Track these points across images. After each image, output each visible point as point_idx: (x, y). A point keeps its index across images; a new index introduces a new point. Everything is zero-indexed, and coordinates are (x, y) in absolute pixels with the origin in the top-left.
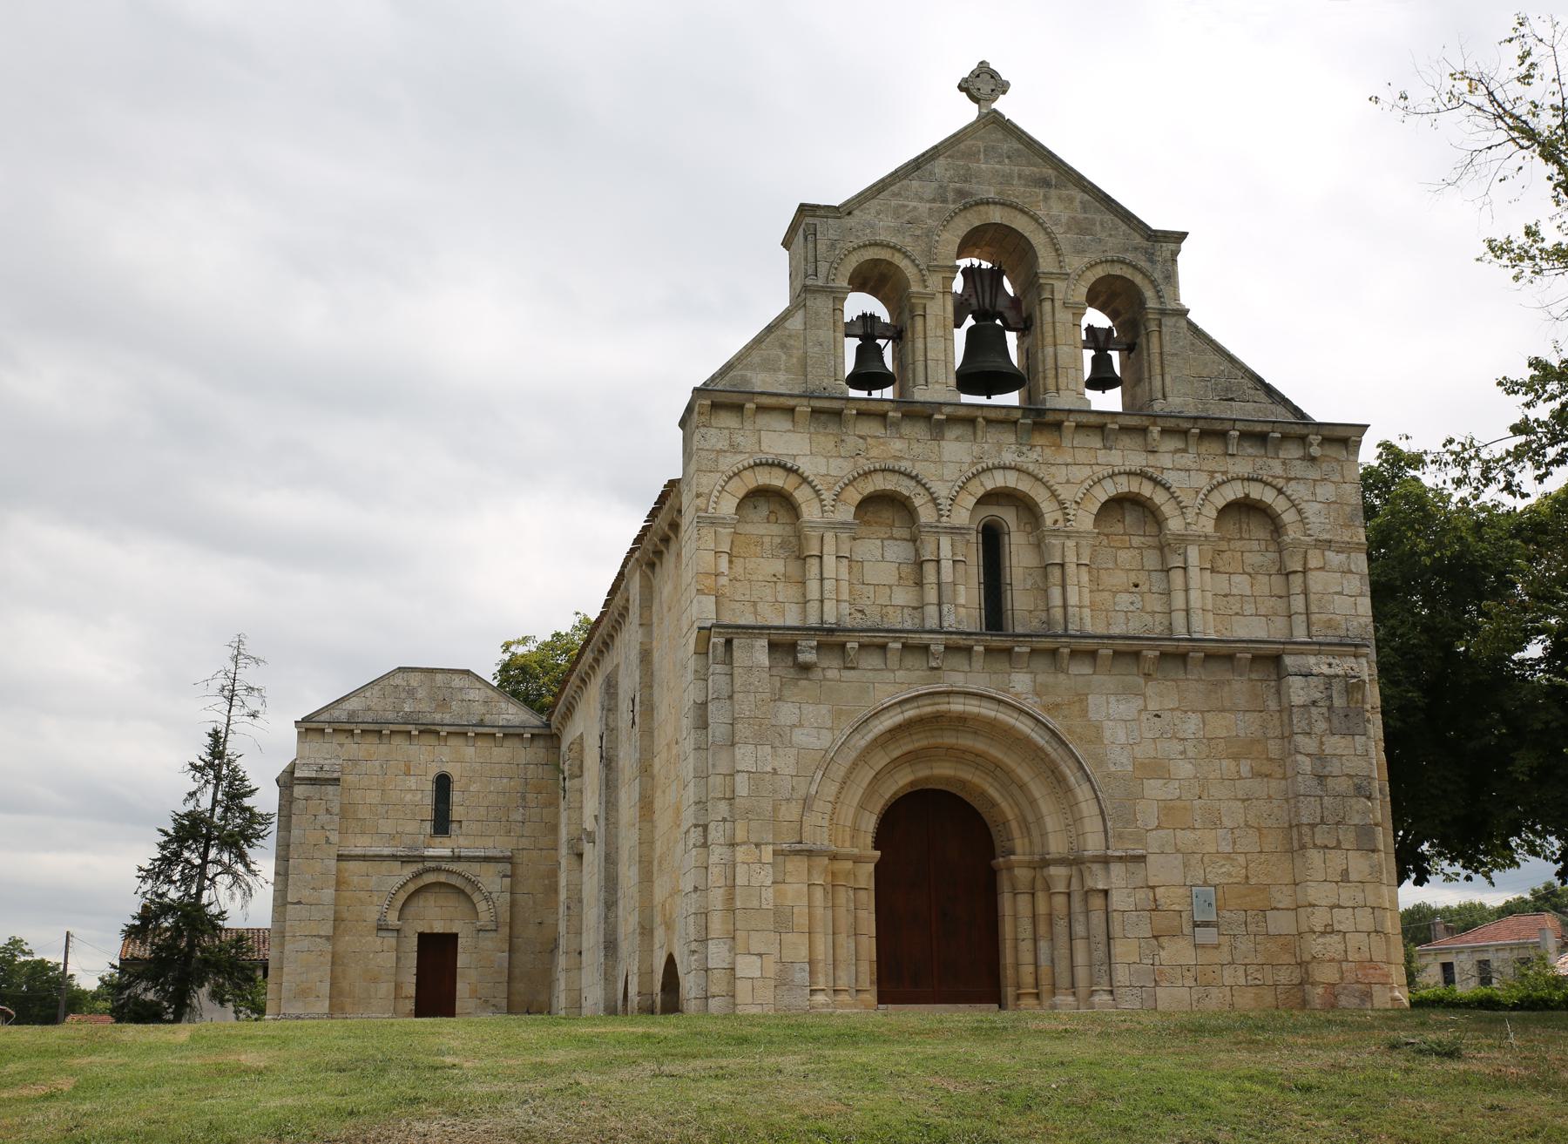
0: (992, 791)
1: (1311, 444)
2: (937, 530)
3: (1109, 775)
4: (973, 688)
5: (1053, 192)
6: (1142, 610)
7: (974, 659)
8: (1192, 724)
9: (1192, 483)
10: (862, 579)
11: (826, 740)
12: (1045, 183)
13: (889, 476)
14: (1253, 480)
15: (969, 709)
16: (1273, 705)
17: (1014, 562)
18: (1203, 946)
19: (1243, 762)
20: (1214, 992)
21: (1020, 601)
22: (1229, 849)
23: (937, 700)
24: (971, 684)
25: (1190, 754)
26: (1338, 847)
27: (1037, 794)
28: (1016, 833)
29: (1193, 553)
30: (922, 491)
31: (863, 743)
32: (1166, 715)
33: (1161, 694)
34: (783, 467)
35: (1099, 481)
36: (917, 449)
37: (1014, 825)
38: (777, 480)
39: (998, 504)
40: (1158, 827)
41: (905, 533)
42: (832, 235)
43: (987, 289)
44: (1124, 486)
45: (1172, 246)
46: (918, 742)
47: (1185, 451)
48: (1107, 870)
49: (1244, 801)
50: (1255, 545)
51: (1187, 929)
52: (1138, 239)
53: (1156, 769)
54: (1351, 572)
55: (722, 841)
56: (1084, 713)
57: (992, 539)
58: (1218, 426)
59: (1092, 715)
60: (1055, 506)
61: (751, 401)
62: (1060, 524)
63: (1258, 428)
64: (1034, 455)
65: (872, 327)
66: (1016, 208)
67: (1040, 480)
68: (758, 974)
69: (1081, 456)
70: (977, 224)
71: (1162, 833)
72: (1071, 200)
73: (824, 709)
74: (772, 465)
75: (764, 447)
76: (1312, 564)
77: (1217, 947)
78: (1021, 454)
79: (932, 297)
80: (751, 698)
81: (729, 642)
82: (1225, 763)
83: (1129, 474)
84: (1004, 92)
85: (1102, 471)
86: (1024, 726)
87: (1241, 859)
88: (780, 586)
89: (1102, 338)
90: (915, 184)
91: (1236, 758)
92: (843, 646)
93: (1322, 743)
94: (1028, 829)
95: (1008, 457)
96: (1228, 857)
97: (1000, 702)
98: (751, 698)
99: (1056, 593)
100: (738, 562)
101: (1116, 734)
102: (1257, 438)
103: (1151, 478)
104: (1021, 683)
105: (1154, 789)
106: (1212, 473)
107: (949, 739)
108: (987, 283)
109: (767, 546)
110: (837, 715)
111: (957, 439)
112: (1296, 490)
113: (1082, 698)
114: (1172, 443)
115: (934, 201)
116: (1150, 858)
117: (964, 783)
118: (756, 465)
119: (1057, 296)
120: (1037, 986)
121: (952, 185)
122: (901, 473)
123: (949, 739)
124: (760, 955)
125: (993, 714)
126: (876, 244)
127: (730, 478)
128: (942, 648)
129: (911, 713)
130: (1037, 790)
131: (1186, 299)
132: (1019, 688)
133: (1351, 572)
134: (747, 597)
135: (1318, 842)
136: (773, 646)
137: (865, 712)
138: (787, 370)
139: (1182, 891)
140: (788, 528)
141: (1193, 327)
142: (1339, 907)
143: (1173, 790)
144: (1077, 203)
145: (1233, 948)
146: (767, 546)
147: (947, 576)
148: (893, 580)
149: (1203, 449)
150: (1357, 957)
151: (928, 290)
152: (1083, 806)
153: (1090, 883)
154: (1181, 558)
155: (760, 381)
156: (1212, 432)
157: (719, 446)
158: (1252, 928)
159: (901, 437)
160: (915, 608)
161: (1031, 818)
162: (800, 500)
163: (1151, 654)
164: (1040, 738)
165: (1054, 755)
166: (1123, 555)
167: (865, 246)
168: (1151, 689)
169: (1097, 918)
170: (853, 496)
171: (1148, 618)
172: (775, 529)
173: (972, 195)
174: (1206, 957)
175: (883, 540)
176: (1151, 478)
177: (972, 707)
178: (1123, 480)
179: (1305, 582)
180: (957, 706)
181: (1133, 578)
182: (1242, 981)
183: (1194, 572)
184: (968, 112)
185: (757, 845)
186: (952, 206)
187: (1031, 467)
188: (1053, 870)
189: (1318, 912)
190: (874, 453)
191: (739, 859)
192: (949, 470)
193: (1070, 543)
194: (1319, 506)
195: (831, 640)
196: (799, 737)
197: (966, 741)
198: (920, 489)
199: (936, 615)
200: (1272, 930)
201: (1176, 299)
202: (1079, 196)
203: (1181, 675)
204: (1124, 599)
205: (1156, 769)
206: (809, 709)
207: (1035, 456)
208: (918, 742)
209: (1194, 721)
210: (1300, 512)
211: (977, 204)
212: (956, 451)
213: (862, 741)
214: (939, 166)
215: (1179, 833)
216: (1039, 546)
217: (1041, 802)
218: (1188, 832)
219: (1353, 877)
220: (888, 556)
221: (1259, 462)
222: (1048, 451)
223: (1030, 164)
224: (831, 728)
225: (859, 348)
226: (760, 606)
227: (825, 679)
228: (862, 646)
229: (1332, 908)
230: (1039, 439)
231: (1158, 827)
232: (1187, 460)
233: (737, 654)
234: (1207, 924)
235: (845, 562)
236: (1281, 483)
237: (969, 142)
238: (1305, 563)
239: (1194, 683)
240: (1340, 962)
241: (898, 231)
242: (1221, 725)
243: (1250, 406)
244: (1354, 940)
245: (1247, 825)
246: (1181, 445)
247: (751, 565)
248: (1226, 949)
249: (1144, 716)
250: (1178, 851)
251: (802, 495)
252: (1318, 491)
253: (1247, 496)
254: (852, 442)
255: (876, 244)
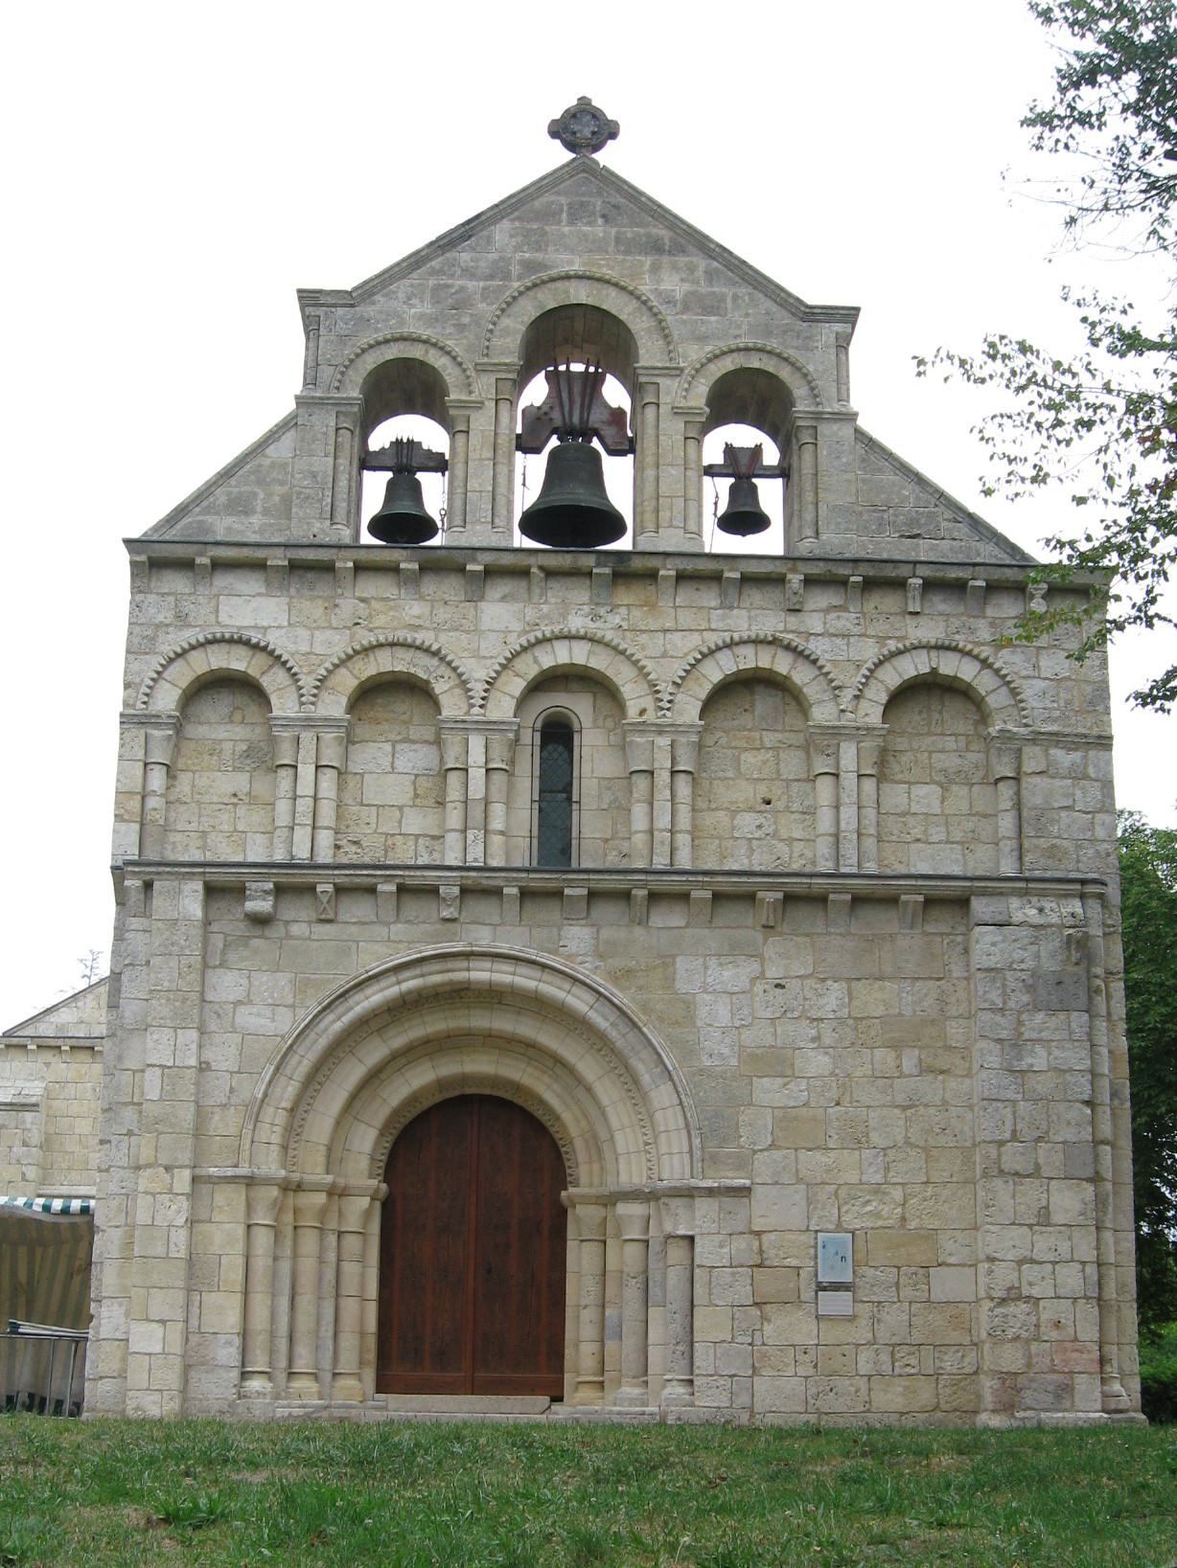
0: (549, 1097)
1: (1032, 597)
2: (464, 727)
3: (701, 1071)
4: (504, 948)
5: (665, 259)
6: (775, 835)
7: (506, 906)
8: (832, 998)
9: (851, 652)
10: (394, 801)
11: (286, 1023)
12: (656, 247)
13: (400, 652)
14: (948, 648)
15: (497, 977)
16: (957, 971)
17: (586, 767)
18: (828, 1318)
19: (907, 1052)
20: (842, 1384)
21: (590, 827)
22: (878, 1178)
23: (450, 965)
24: (500, 944)
25: (827, 1041)
26: (1036, 1173)
27: (605, 1100)
28: (581, 1155)
29: (848, 754)
30: (448, 673)
31: (338, 1026)
32: (793, 985)
33: (787, 956)
34: (246, 643)
35: (712, 652)
36: (443, 614)
37: (579, 1144)
38: (238, 661)
39: (567, 691)
40: (772, 1146)
41: (428, 733)
42: (342, 328)
43: (578, 400)
44: (749, 659)
45: (838, 327)
46: (434, 1024)
47: (845, 609)
48: (692, 1207)
49: (905, 1108)
50: (950, 743)
51: (808, 1294)
52: (784, 318)
53: (776, 1062)
54: (1086, 777)
55: (124, 1162)
56: (669, 981)
57: (558, 735)
58: (890, 572)
59: (682, 986)
60: (644, 688)
61: (474, 561)
62: (650, 716)
63: (953, 574)
64: (616, 619)
65: (410, 458)
66: (608, 282)
67: (623, 653)
68: (158, 1349)
69: (686, 618)
70: (552, 305)
71: (777, 1154)
72: (691, 269)
73: (283, 979)
74: (231, 641)
75: (223, 618)
76: (1029, 766)
77: (852, 1318)
78: (595, 618)
79: (479, 405)
80: (174, 963)
81: (148, 886)
82: (879, 1053)
83: (757, 642)
84: (554, 122)
85: (713, 639)
86: (578, 1001)
87: (897, 1194)
88: (241, 811)
89: (744, 461)
90: (465, 256)
91: (896, 1046)
92: (311, 889)
93: (1020, 1023)
94: (599, 1151)
95: (577, 623)
96: (877, 1190)
97: (544, 966)
98: (174, 963)
99: (639, 812)
100: (184, 781)
101: (715, 1014)
102: (945, 585)
103: (788, 648)
104: (576, 941)
105: (769, 1091)
106: (881, 640)
107: (480, 1020)
108: (577, 389)
109: (227, 755)
110: (301, 987)
111: (503, 599)
112: (1009, 660)
113: (667, 961)
114: (821, 599)
115: (492, 277)
116: (758, 1191)
117: (517, 1087)
118: (209, 642)
119: (664, 399)
120: (602, 1372)
121: (518, 256)
122: (418, 648)
123: (480, 1020)
124: (163, 1322)
125: (531, 984)
126: (403, 339)
127: (171, 660)
128: (456, 890)
129: (410, 983)
130: (608, 1092)
131: (856, 403)
132: (573, 947)
133: (1086, 777)
134: (194, 826)
135: (1006, 1167)
136: (212, 891)
137: (342, 982)
138: (266, 512)
139: (803, 1237)
140: (258, 730)
141: (861, 436)
142: (1033, 1261)
143: (798, 1092)
144: (700, 273)
145: (875, 1320)
146: (227, 755)
147: (477, 790)
148: (406, 798)
149: (869, 606)
150: (1054, 1335)
151: (473, 398)
152: (659, 1115)
153: (668, 1228)
154: (831, 761)
155: (223, 527)
156: (879, 580)
157: (160, 618)
158: (906, 1292)
159: (422, 598)
160: (434, 838)
161: (603, 1135)
162: (626, 696)
163: (771, 896)
164: (601, 1019)
165: (620, 1043)
166: (750, 759)
167: (387, 341)
168: (772, 947)
169: (675, 1278)
170: (348, 681)
171: (782, 849)
172: (240, 732)
173: (544, 267)
174: (832, 1334)
175: (394, 743)
176: (788, 648)
177: (503, 975)
178: (748, 651)
179: (1018, 793)
180: (481, 973)
181: (763, 791)
182: (887, 1368)
183: (849, 780)
184: (559, 155)
185: (168, 1169)
186: (516, 284)
187: (609, 636)
188: (622, 1208)
189: (1000, 1269)
190: (380, 621)
191: (141, 1189)
192: (486, 643)
193: (663, 741)
194: (1043, 684)
195: (293, 884)
196: (247, 1018)
197: (525, 1028)
198: (443, 670)
199: (460, 846)
200: (937, 1295)
201: (843, 396)
202: (702, 263)
203: (820, 928)
204: (747, 822)
205: (776, 1062)
206: (262, 979)
207: (617, 620)
208: (434, 1024)
209: (836, 992)
210: (1014, 693)
211: (553, 280)
212: (502, 617)
213: (335, 1024)
214: (502, 233)
215: (803, 1155)
216: (623, 748)
217: (610, 1111)
218: (818, 1155)
219: (1058, 1218)
220: (402, 764)
221: (956, 623)
222: (636, 613)
223: (633, 224)
224: (293, 1006)
225: (732, 488)
226: (212, 837)
227: (289, 936)
228: (340, 890)
229: (1020, 1263)
230: (625, 596)
231: (772, 1146)
232: (845, 621)
233: (158, 902)
234: (837, 1287)
235: (331, 774)
236: (985, 652)
237: (544, 200)
238: (1019, 767)
239: (838, 939)
240: (1028, 1342)
241: (431, 320)
242: (875, 999)
243: (945, 544)
244: (1048, 1312)
245: (907, 1143)
246: (837, 601)
247: (202, 781)
248: (864, 1322)
249: (759, 988)
250: (799, 1181)
251: (273, 681)
252: (1044, 662)
253: (934, 671)
254: (348, 606)
255: (403, 339)
